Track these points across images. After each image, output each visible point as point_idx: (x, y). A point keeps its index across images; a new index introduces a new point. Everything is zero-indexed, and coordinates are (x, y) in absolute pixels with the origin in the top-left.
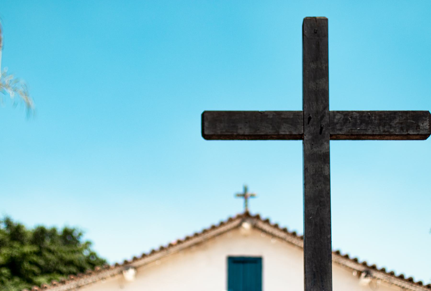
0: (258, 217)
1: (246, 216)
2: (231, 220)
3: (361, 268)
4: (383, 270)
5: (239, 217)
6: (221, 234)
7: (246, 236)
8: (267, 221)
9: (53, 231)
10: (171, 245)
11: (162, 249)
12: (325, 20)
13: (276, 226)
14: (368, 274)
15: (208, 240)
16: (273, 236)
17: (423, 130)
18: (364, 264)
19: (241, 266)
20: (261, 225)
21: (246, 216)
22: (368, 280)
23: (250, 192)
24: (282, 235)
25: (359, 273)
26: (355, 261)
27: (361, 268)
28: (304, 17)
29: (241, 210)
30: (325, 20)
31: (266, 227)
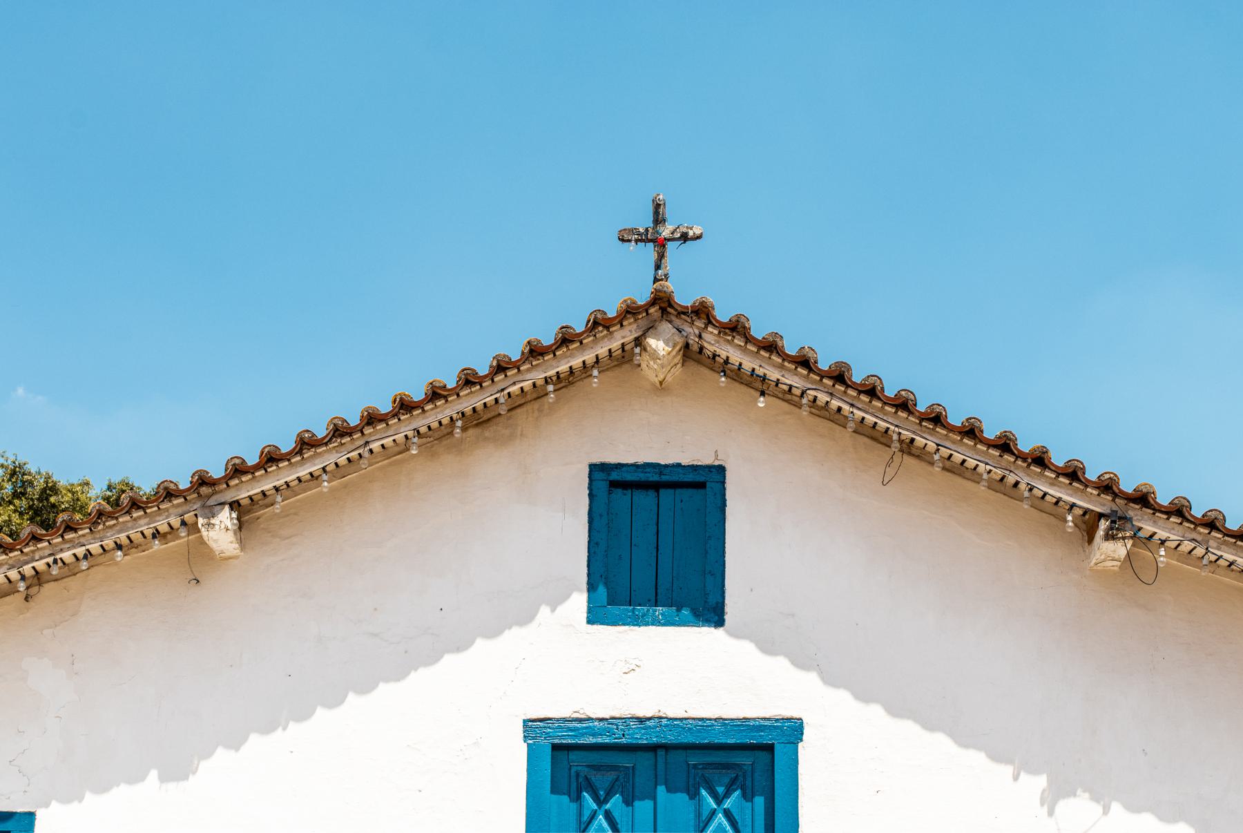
0: (702, 312)
1: (663, 304)
2: (599, 324)
3: (1099, 504)
4: (1179, 511)
5: (630, 311)
6: (565, 381)
7: (662, 387)
8: (736, 328)
12: (590, 621)
13: (771, 346)
14: (1118, 524)
15: (518, 403)
16: (760, 385)
17: (30, 472)
18: (1107, 487)
19: (645, 499)
20: (713, 343)
21: (663, 304)
22: (1119, 549)
23: (644, 221)
24: (795, 380)
25: (1088, 524)
26: (1073, 474)
27: (1099, 504)
28: (710, 300)
30: (590, 621)
31: (732, 352)
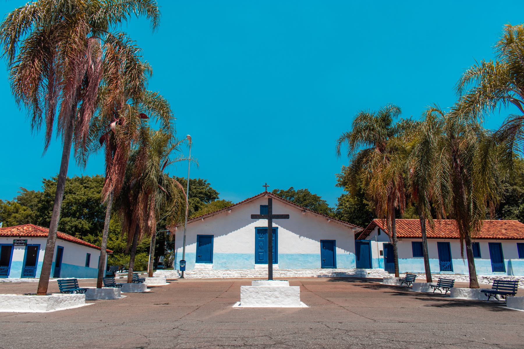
1: (267, 192)
2: (261, 194)
5: (264, 193)
9: (195, 180)
10: (242, 202)
11: (240, 203)
19: (265, 208)
22: (304, 213)
29: (264, 191)
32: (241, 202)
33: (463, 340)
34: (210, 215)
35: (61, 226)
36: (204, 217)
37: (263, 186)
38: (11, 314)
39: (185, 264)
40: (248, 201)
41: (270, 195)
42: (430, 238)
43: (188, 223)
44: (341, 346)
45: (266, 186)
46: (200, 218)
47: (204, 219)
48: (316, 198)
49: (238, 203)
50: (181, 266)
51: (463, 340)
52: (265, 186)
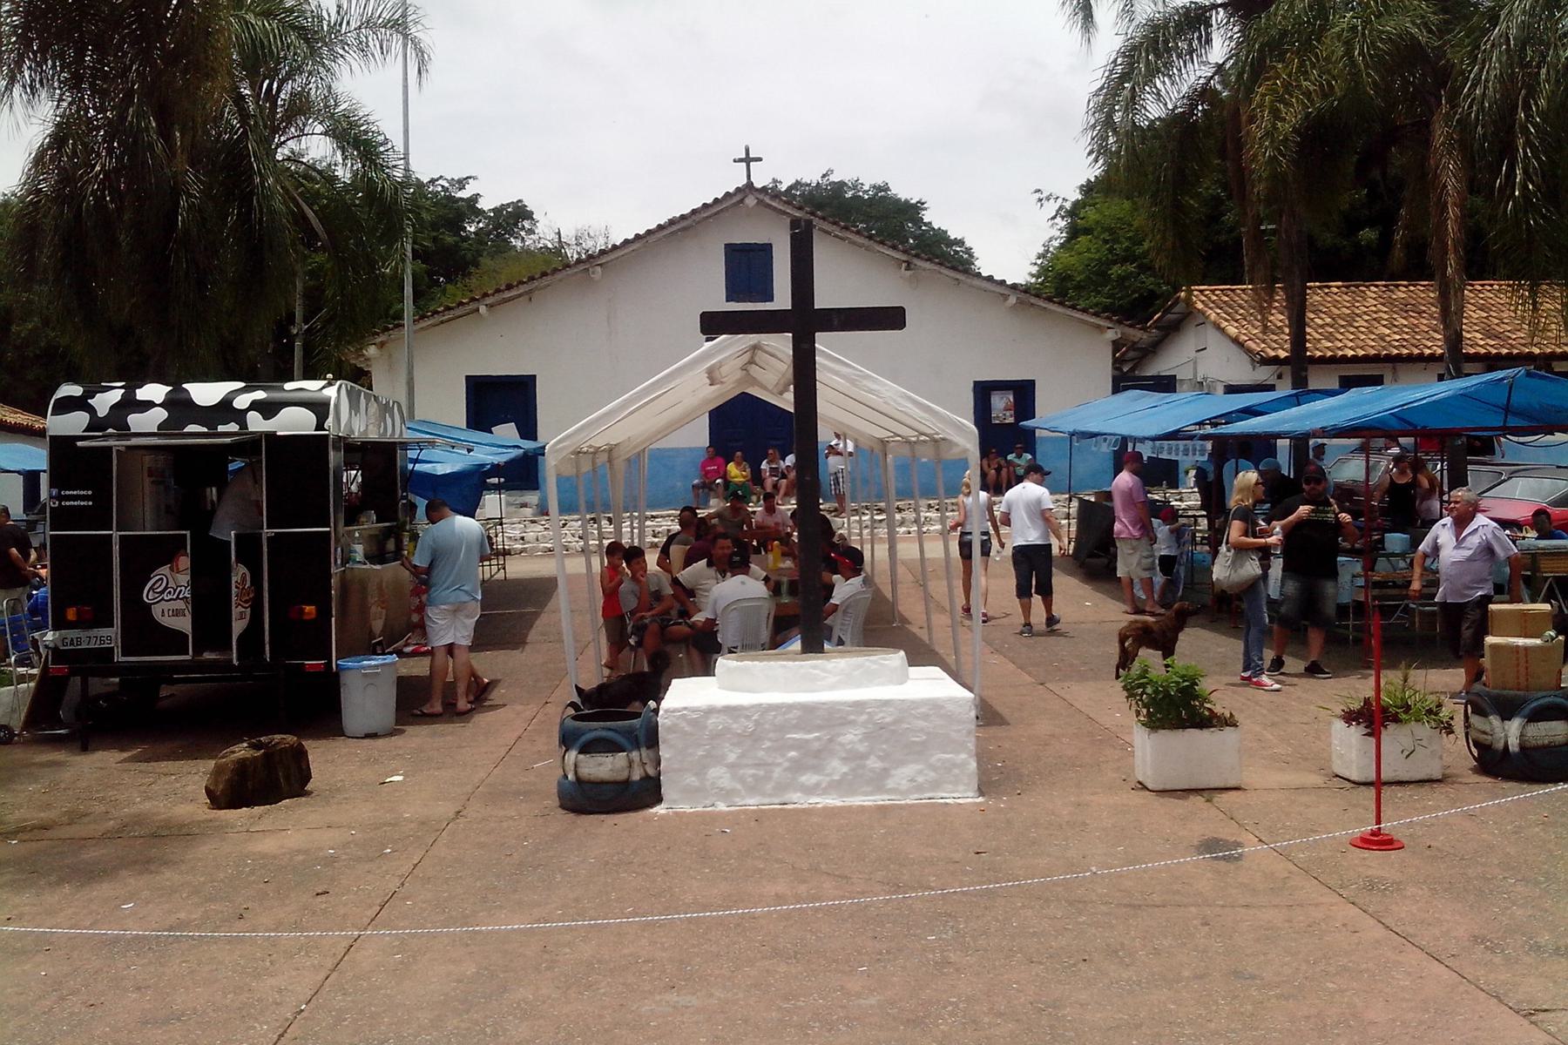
1: (750, 185)
29: (743, 181)
32: (642, 232)
33: (140, 772)
34: (514, 293)
35: (328, 262)
36: (489, 301)
37: (760, 159)
38: (184, 831)
39: (1136, 440)
40: (675, 228)
41: (767, 200)
42: (1323, 360)
43: (415, 332)
44: (1324, 926)
45: (748, 160)
46: (472, 306)
47: (490, 306)
48: (912, 211)
49: (631, 237)
50: (1279, 436)
51: (140, 772)
52: (741, 160)
